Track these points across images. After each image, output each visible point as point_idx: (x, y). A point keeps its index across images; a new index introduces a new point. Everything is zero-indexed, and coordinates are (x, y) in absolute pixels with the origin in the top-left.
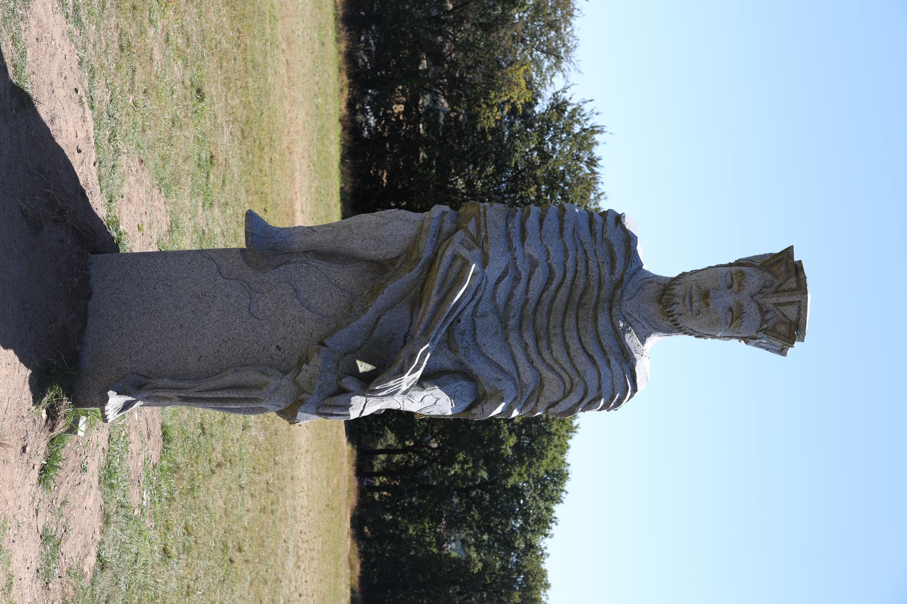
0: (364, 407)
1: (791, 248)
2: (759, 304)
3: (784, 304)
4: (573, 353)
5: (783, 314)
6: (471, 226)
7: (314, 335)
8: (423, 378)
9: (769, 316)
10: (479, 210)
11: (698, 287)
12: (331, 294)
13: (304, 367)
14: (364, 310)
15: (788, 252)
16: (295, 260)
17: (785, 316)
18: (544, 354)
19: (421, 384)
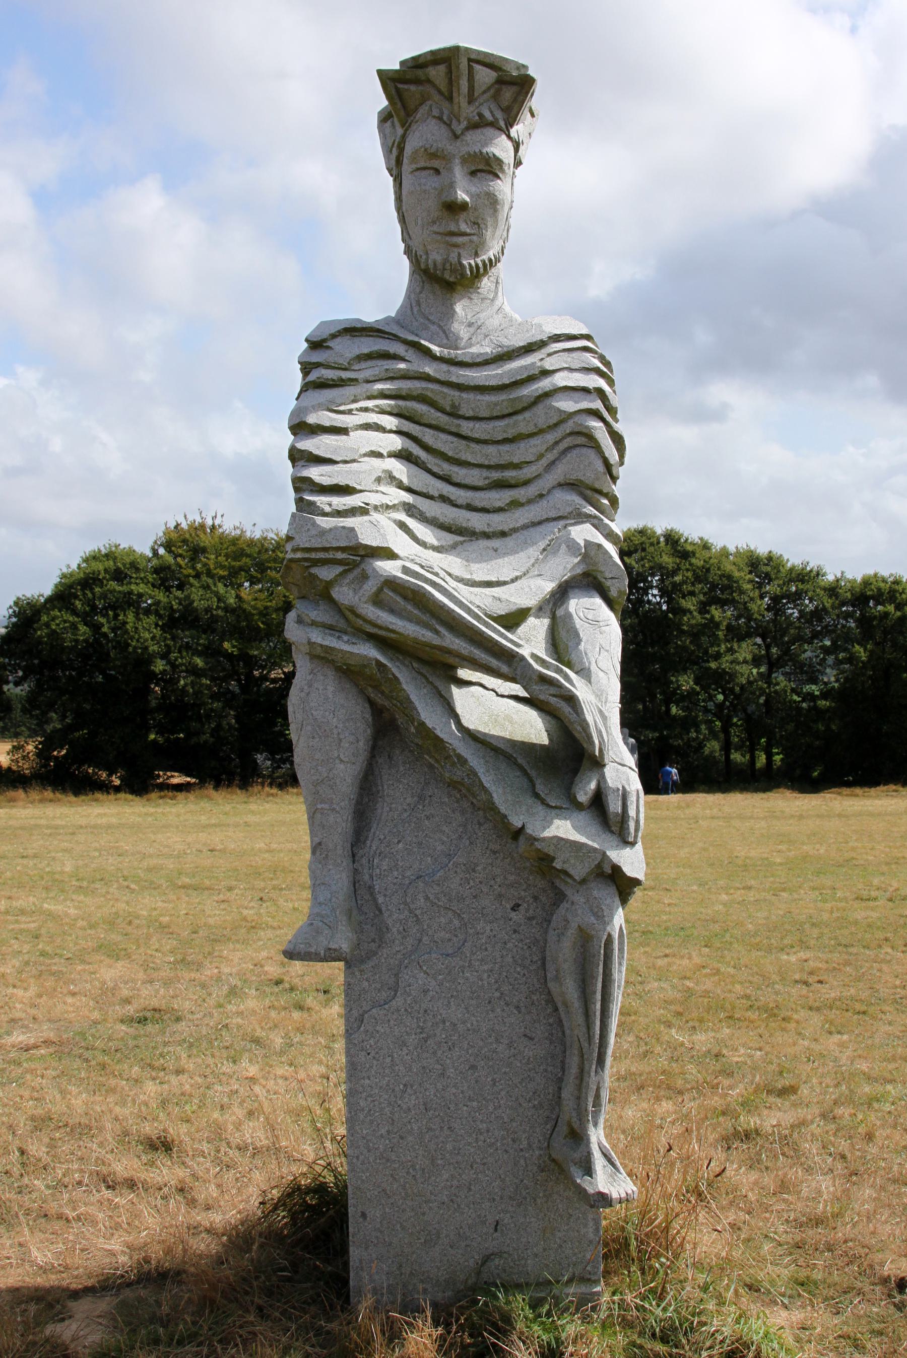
0: (624, 765)
1: (380, 73)
2: (467, 129)
3: (471, 88)
4: (531, 429)
5: (484, 92)
6: (326, 573)
7: (497, 847)
8: (569, 665)
9: (487, 115)
10: (299, 560)
11: (434, 222)
12: (428, 818)
13: (558, 865)
14: (463, 761)
15: (388, 80)
16: (367, 877)
17: (489, 89)
18: (529, 476)
19: (585, 673)
